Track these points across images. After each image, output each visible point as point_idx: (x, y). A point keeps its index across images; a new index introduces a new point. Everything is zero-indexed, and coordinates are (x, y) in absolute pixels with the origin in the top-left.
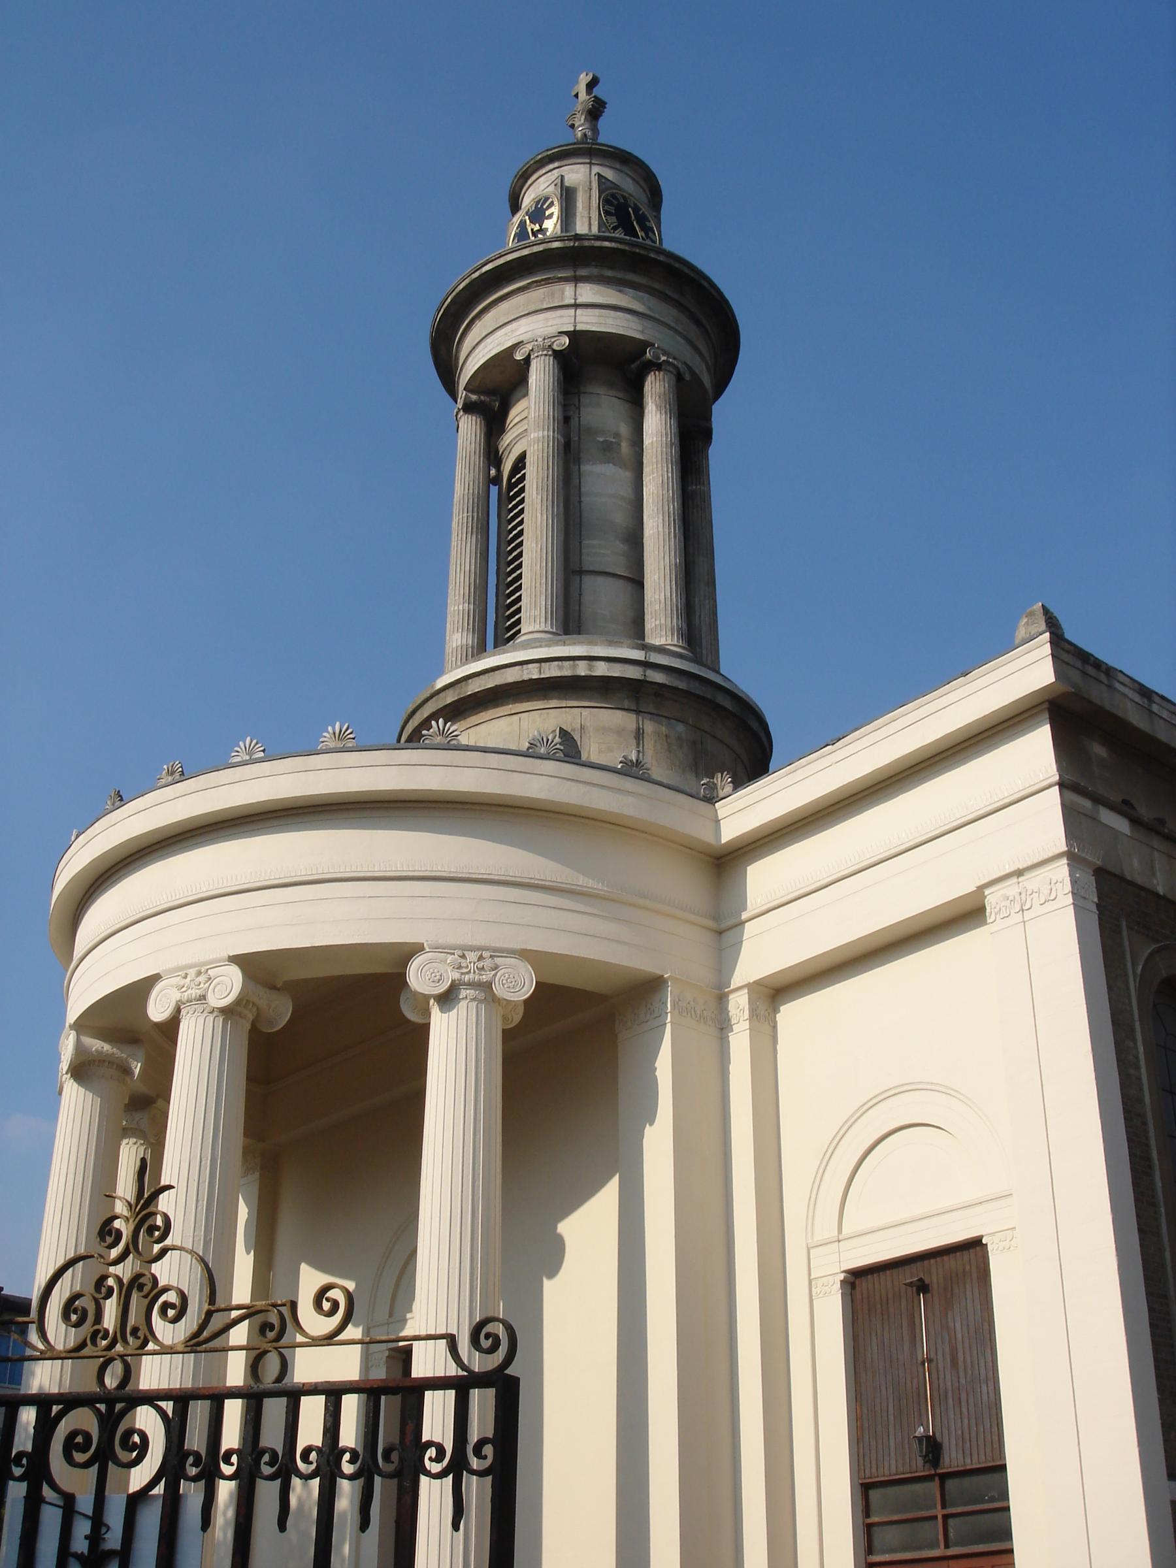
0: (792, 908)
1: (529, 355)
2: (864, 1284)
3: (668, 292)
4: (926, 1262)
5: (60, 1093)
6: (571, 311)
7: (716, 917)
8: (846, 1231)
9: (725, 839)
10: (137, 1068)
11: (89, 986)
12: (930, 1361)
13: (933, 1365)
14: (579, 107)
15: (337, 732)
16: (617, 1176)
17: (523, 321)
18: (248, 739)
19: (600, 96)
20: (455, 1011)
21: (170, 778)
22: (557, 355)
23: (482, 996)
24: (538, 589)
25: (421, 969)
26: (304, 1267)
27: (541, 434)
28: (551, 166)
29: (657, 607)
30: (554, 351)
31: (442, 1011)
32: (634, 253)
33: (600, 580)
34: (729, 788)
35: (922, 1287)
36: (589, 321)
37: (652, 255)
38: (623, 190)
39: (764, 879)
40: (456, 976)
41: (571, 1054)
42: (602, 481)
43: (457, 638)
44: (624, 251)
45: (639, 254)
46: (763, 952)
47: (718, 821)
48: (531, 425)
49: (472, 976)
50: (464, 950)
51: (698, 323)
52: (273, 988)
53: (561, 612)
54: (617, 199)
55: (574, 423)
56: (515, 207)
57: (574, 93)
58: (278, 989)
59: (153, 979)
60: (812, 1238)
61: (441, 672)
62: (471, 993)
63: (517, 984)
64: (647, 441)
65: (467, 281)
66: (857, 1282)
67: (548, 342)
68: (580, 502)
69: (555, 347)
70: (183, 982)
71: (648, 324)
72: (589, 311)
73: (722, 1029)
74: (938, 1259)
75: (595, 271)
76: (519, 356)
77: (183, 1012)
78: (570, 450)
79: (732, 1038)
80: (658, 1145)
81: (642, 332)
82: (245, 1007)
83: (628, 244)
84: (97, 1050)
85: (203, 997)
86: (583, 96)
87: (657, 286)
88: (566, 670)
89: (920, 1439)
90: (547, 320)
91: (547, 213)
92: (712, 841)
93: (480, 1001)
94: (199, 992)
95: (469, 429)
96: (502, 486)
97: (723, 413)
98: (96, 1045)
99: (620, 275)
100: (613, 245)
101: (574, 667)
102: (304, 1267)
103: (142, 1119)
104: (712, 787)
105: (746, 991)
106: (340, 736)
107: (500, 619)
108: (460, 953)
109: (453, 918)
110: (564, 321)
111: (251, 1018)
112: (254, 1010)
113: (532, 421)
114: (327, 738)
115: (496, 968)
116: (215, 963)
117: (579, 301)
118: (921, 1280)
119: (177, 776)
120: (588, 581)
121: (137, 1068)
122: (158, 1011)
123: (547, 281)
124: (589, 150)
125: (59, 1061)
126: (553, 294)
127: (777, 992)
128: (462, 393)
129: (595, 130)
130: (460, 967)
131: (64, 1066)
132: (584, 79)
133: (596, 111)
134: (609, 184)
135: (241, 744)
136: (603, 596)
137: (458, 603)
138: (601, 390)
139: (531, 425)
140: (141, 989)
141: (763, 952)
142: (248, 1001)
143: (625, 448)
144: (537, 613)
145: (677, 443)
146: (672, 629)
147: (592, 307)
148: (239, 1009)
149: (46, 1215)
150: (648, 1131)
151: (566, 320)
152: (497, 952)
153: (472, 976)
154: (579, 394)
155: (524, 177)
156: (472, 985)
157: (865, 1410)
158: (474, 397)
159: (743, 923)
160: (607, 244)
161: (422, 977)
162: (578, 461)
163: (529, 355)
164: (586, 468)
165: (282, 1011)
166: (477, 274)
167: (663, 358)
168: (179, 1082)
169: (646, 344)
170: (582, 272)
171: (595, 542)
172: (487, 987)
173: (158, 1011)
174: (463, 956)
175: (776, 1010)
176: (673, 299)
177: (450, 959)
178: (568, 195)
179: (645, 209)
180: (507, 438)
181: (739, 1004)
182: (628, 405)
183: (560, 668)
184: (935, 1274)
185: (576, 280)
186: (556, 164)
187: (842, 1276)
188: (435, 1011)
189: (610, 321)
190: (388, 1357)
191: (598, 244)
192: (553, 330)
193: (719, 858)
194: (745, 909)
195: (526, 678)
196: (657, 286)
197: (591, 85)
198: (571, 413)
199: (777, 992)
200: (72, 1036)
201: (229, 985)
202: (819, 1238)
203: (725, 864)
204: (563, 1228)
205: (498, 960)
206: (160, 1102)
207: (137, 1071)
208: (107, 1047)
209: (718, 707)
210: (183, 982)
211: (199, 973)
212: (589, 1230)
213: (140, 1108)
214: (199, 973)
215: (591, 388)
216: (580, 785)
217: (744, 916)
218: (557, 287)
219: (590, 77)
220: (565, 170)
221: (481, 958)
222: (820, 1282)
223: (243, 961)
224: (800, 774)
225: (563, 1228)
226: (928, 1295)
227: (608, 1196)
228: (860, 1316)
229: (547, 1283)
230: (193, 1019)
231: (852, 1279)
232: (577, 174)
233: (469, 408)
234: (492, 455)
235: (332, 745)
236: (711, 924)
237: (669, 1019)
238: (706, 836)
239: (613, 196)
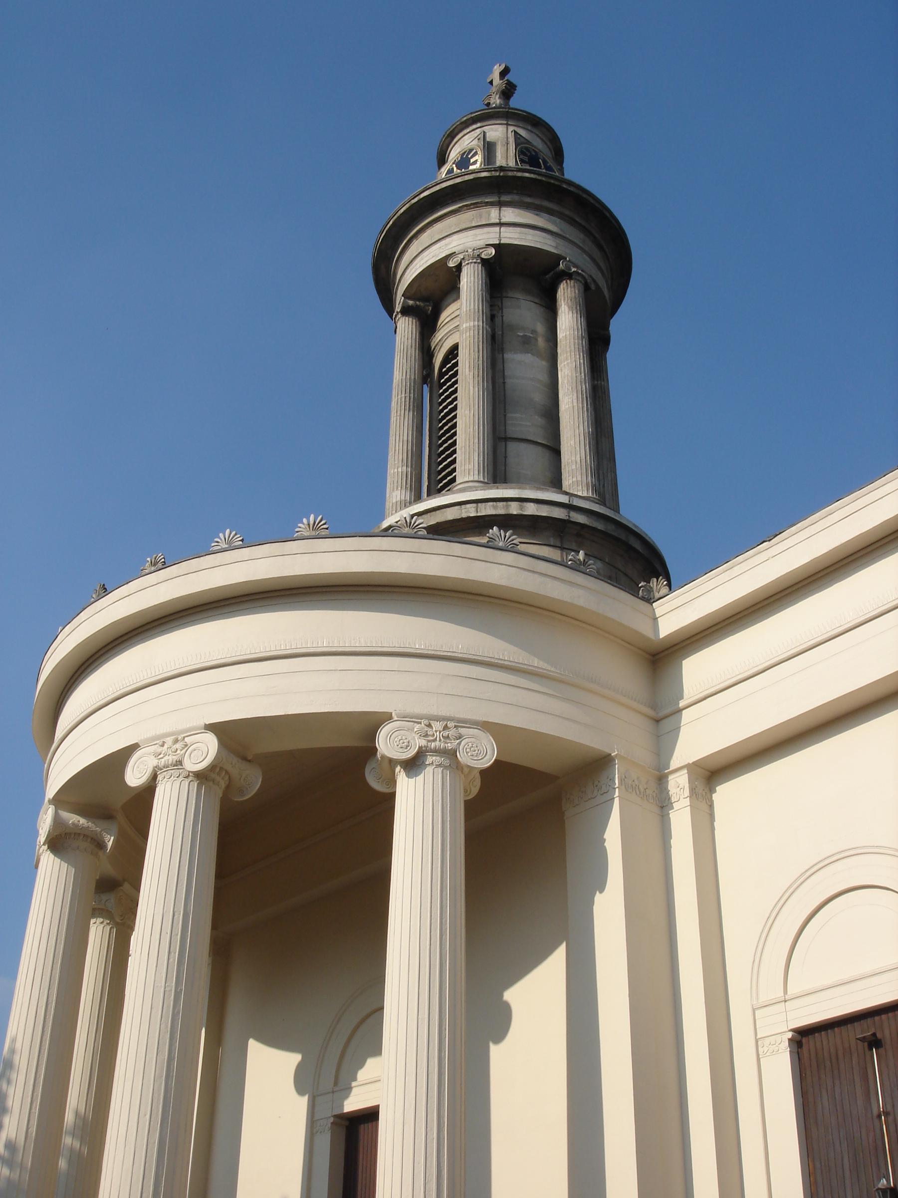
0: (727, 694)
1: (460, 264)
2: (809, 1042)
3: (577, 220)
4: (877, 1018)
5: (37, 867)
6: (497, 229)
7: (654, 706)
8: (792, 990)
9: (661, 636)
10: (110, 841)
11: (68, 762)
12: (887, 1114)
13: (890, 1118)
14: (494, 89)
15: (312, 522)
16: (564, 945)
17: (455, 237)
18: (228, 531)
19: (512, 80)
20: (422, 775)
21: (153, 568)
22: (485, 262)
23: (447, 762)
24: (472, 446)
25: (390, 735)
26: (252, 1043)
27: (472, 324)
28: (474, 126)
29: (574, 467)
30: (482, 259)
31: (408, 776)
32: (549, 183)
33: (523, 446)
34: (665, 590)
35: (874, 1042)
36: (511, 237)
37: (565, 186)
38: (533, 146)
39: (698, 671)
40: (423, 742)
41: (527, 827)
42: (523, 367)
43: (395, 493)
44: (540, 181)
45: (554, 184)
46: (701, 734)
47: (655, 619)
48: (462, 323)
50: (431, 719)
51: (601, 248)
52: (245, 759)
53: (491, 467)
54: (529, 151)
55: (498, 320)
56: (442, 160)
57: (489, 80)
58: (249, 761)
59: (131, 749)
60: (758, 998)
61: (383, 519)
63: (480, 753)
64: (560, 335)
65: (407, 206)
66: (804, 1040)
67: (477, 252)
68: (504, 383)
69: (483, 256)
70: (160, 749)
71: (561, 242)
72: (511, 229)
73: (662, 807)
74: (890, 1014)
75: (516, 198)
76: (452, 264)
77: (160, 778)
78: (496, 341)
79: (673, 815)
80: (609, 912)
81: (556, 248)
82: (219, 774)
83: (539, 180)
84: (73, 824)
85: (179, 763)
86: (497, 81)
87: (567, 212)
88: (500, 509)
89: (884, 1191)
90: (476, 235)
91: (472, 161)
92: (652, 636)
93: (445, 767)
94: (175, 758)
95: (406, 328)
96: (435, 377)
97: (617, 326)
98: (72, 819)
99: (537, 202)
100: (532, 176)
101: (507, 507)
102: (252, 1043)
103: (110, 900)
104: (650, 590)
105: (686, 771)
106: (315, 527)
107: (432, 481)
108: (426, 722)
109: (421, 690)
110: (491, 236)
111: (223, 784)
112: (227, 777)
113: (463, 315)
114: (302, 527)
115: (460, 737)
116: (192, 731)
117: (504, 220)
118: (874, 1035)
119: (160, 565)
120: (512, 447)
121: (110, 841)
122: (135, 776)
123: (476, 205)
124: (506, 115)
125: (36, 834)
126: (481, 216)
127: (713, 773)
128: (399, 301)
129: (507, 104)
130: (426, 735)
131: (42, 838)
132: (497, 69)
133: (508, 92)
134: (522, 140)
135: (221, 535)
136: (527, 458)
137: (396, 467)
138: (518, 295)
139: (462, 323)
140: (118, 760)
141: (701, 734)
142: (221, 768)
143: (541, 343)
144: (471, 467)
145: (586, 336)
146: (587, 484)
147: (514, 226)
148: (213, 776)
149: (10, 1025)
150: (599, 899)
151: (492, 235)
152: (462, 723)
153: (437, 743)
154: (501, 298)
155: (451, 136)
157: (818, 1165)
158: (411, 302)
159: (680, 711)
160: (527, 175)
161: (389, 744)
162: (502, 351)
163: (460, 264)
164: (508, 356)
165: (252, 781)
166: (416, 200)
167: (574, 269)
168: (154, 844)
169: (559, 258)
170: (505, 198)
171: (518, 415)
173: (135, 776)
174: (429, 726)
175: (712, 791)
176: (580, 225)
177: (417, 727)
178: (489, 148)
179: (551, 163)
180: (439, 335)
181: (679, 785)
182: (542, 309)
183: (495, 508)
184: (886, 1028)
185: (501, 204)
186: (479, 125)
187: (790, 1035)
188: (402, 779)
189: (530, 237)
191: (519, 174)
192: (482, 243)
193: (654, 655)
194: (682, 698)
195: (464, 515)
196: (567, 212)
197: (504, 73)
198: (495, 312)
199: (713, 773)
200: (51, 810)
201: (205, 751)
202: (764, 998)
203: (661, 659)
204: (510, 995)
205: (462, 730)
206: (126, 886)
207: (110, 844)
208: (82, 821)
209: (630, 548)
210: (160, 749)
211: (176, 741)
212: (537, 997)
213: (111, 891)
214: (176, 741)
215: (510, 294)
216: (536, 576)
217: (682, 704)
218: (484, 211)
219: (503, 67)
220: (485, 129)
221: (446, 728)
222: (767, 1041)
223: (218, 729)
224: (737, 570)
225: (510, 995)
226: (881, 1050)
227: (553, 969)
228: (808, 1073)
229: (494, 1049)
230: (169, 784)
231: (799, 1038)
232: (496, 132)
233: (406, 311)
234: (426, 352)
235: (306, 534)
236: (650, 712)
237: (617, 794)
238: (645, 629)
239: (526, 148)
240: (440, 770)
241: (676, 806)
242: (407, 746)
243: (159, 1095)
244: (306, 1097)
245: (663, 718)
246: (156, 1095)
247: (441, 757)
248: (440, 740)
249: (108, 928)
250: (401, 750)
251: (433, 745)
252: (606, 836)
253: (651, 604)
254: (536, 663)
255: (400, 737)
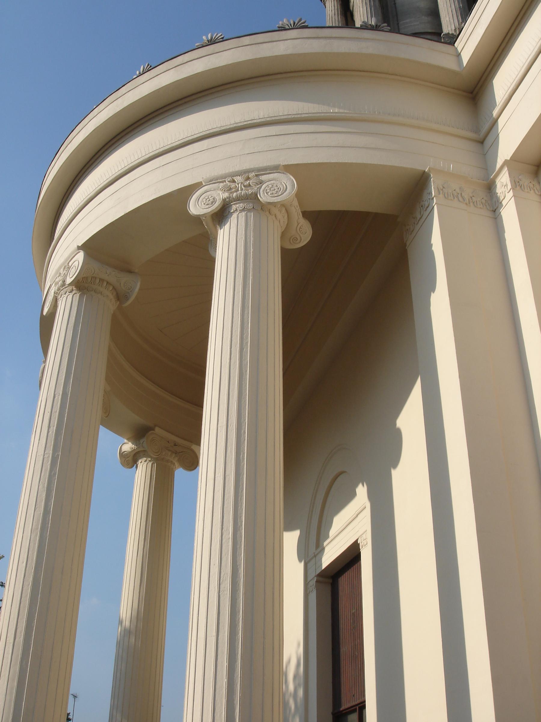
7: (477, 130)
23: (250, 206)
40: (226, 195)
49: (243, 192)
62: (241, 205)
63: (281, 189)
73: (494, 211)
93: (249, 210)
156: (239, 199)
159: (495, 122)
171: (408, 21)
172: (254, 198)
174: (234, 181)
190: (316, 582)
193: (472, 93)
203: (474, 91)
205: (263, 178)
238: (449, 63)
240: (244, 214)
241: (504, 203)
242: (212, 202)
243: (35, 544)
244: (303, 562)
245: (483, 138)
246: (32, 544)
247: (244, 203)
248: (242, 189)
249: (150, 464)
250: (207, 206)
251: (235, 194)
252: (432, 242)
253: (452, 43)
254: (333, 110)
255: (206, 198)
